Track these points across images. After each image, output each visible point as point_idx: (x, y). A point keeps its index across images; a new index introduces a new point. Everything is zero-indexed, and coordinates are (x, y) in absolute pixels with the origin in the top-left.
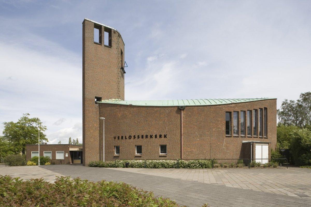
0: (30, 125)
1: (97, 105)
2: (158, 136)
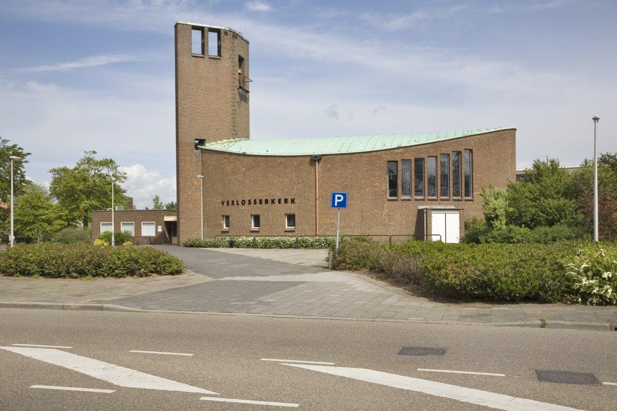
0: (96, 171)
1: (199, 151)
2: (283, 201)
